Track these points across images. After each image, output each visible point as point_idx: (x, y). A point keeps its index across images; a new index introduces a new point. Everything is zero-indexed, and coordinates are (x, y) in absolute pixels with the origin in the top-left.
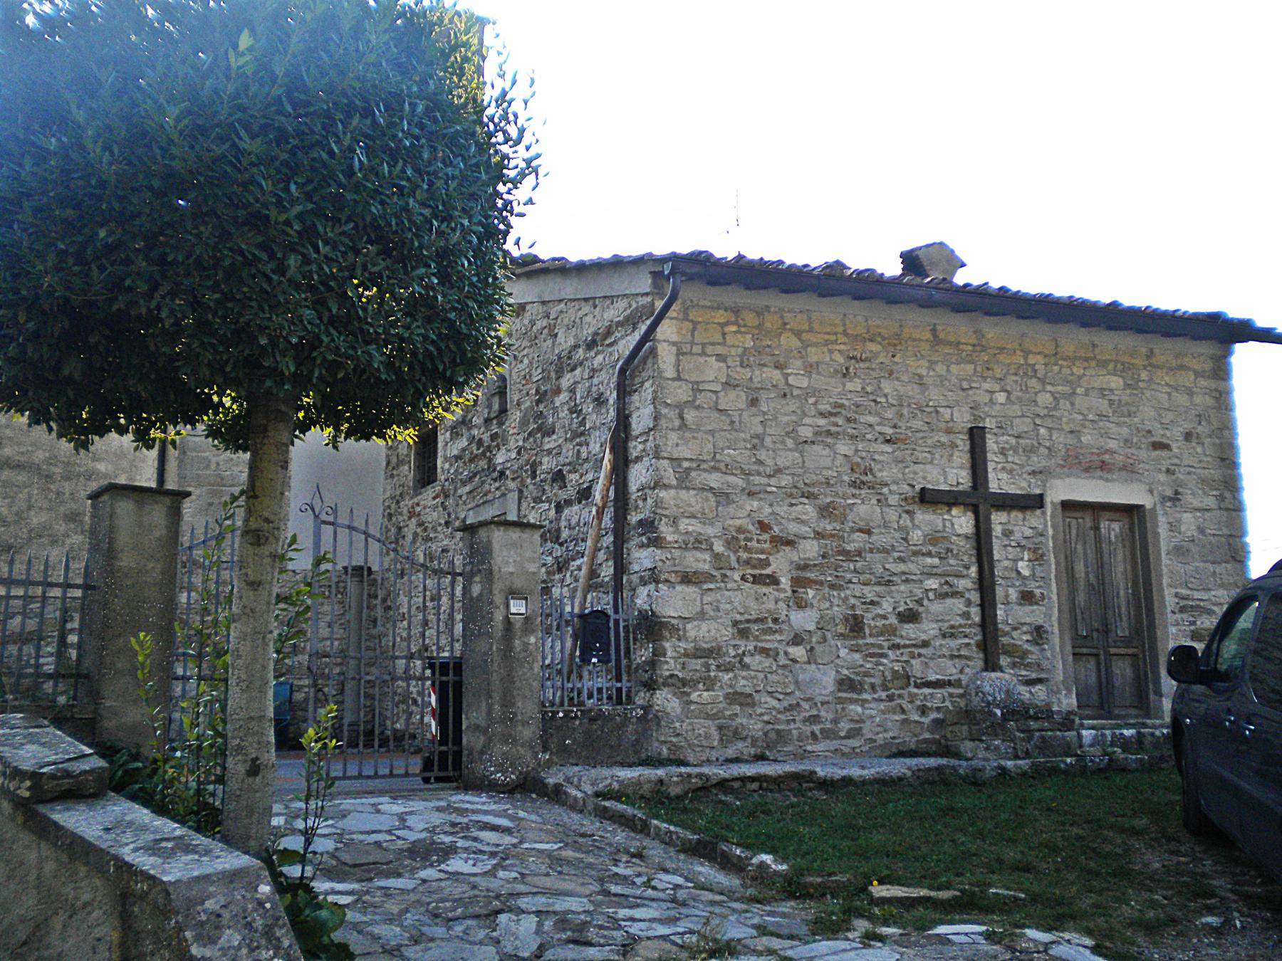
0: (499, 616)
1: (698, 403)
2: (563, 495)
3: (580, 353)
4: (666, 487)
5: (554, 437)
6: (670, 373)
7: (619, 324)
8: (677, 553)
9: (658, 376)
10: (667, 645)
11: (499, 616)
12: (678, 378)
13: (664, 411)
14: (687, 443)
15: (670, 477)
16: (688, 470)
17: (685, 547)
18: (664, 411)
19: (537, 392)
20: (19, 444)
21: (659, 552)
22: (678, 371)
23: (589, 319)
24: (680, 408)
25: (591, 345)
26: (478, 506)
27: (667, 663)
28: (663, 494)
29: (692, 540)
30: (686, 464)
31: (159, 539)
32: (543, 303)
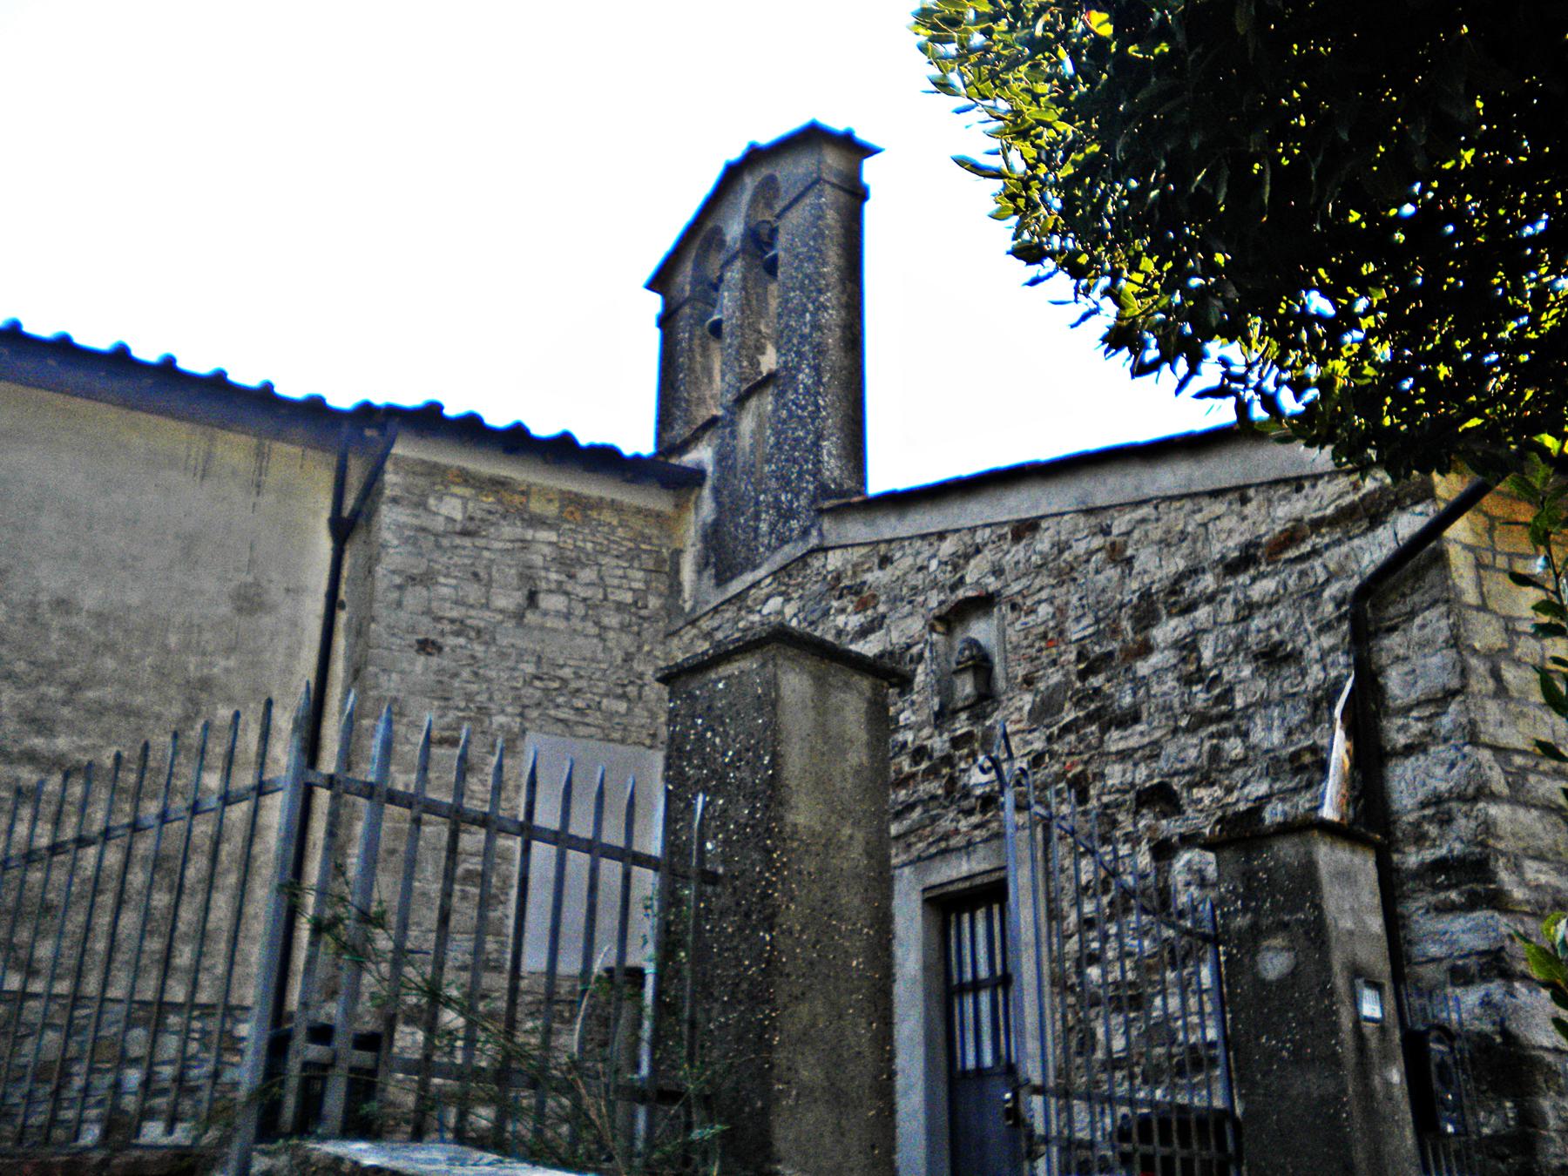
0: (1346, 1022)
1: (1517, 653)
2: (1171, 827)
3: (1208, 582)
4: (1494, 797)
5: (1140, 728)
6: (1471, 597)
7: (1316, 525)
8: (1531, 924)
9: (1449, 600)
10: (1546, 1104)
11: (1346, 1022)
12: (1483, 608)
13: (1474, 662)
14: (1514, 724)
15: (1498, 781)
16: (1523, 772)
17: (1538, 913)
18: (1474, 662)
19: (1081, 656)
20: (82, 733)
21: (1504, 920)
22: (1482, 594)
23: (1225, 523)
24: (1493, 659)
25: (1232, 568)
26: (919, 859)
27: (1551, 1140)
28: (1493, 810)
29: (1548, 899)
30: (1518, 760)
31: (857, 773)
32: (1090, 512)
